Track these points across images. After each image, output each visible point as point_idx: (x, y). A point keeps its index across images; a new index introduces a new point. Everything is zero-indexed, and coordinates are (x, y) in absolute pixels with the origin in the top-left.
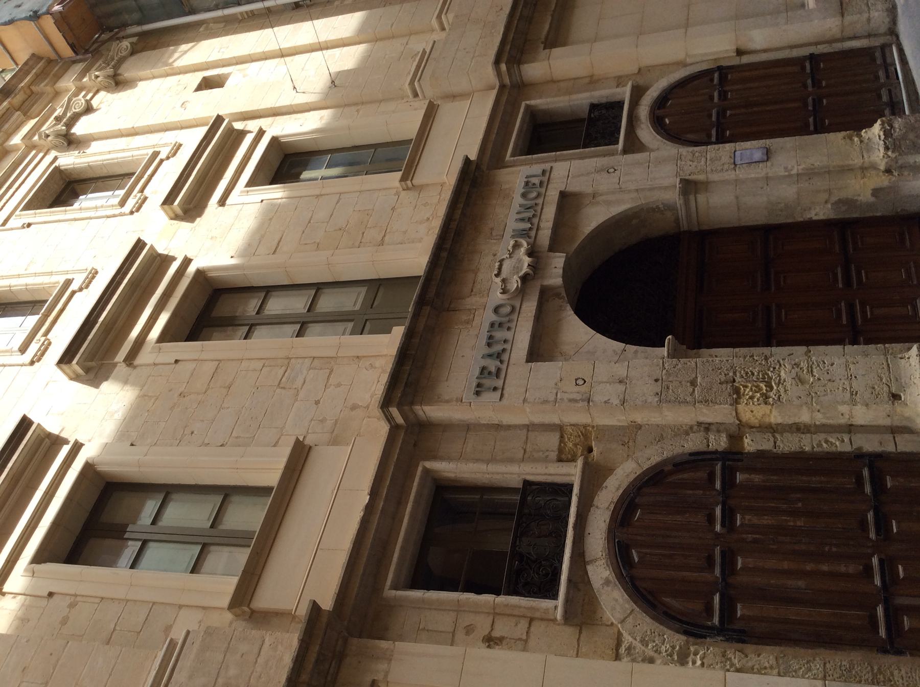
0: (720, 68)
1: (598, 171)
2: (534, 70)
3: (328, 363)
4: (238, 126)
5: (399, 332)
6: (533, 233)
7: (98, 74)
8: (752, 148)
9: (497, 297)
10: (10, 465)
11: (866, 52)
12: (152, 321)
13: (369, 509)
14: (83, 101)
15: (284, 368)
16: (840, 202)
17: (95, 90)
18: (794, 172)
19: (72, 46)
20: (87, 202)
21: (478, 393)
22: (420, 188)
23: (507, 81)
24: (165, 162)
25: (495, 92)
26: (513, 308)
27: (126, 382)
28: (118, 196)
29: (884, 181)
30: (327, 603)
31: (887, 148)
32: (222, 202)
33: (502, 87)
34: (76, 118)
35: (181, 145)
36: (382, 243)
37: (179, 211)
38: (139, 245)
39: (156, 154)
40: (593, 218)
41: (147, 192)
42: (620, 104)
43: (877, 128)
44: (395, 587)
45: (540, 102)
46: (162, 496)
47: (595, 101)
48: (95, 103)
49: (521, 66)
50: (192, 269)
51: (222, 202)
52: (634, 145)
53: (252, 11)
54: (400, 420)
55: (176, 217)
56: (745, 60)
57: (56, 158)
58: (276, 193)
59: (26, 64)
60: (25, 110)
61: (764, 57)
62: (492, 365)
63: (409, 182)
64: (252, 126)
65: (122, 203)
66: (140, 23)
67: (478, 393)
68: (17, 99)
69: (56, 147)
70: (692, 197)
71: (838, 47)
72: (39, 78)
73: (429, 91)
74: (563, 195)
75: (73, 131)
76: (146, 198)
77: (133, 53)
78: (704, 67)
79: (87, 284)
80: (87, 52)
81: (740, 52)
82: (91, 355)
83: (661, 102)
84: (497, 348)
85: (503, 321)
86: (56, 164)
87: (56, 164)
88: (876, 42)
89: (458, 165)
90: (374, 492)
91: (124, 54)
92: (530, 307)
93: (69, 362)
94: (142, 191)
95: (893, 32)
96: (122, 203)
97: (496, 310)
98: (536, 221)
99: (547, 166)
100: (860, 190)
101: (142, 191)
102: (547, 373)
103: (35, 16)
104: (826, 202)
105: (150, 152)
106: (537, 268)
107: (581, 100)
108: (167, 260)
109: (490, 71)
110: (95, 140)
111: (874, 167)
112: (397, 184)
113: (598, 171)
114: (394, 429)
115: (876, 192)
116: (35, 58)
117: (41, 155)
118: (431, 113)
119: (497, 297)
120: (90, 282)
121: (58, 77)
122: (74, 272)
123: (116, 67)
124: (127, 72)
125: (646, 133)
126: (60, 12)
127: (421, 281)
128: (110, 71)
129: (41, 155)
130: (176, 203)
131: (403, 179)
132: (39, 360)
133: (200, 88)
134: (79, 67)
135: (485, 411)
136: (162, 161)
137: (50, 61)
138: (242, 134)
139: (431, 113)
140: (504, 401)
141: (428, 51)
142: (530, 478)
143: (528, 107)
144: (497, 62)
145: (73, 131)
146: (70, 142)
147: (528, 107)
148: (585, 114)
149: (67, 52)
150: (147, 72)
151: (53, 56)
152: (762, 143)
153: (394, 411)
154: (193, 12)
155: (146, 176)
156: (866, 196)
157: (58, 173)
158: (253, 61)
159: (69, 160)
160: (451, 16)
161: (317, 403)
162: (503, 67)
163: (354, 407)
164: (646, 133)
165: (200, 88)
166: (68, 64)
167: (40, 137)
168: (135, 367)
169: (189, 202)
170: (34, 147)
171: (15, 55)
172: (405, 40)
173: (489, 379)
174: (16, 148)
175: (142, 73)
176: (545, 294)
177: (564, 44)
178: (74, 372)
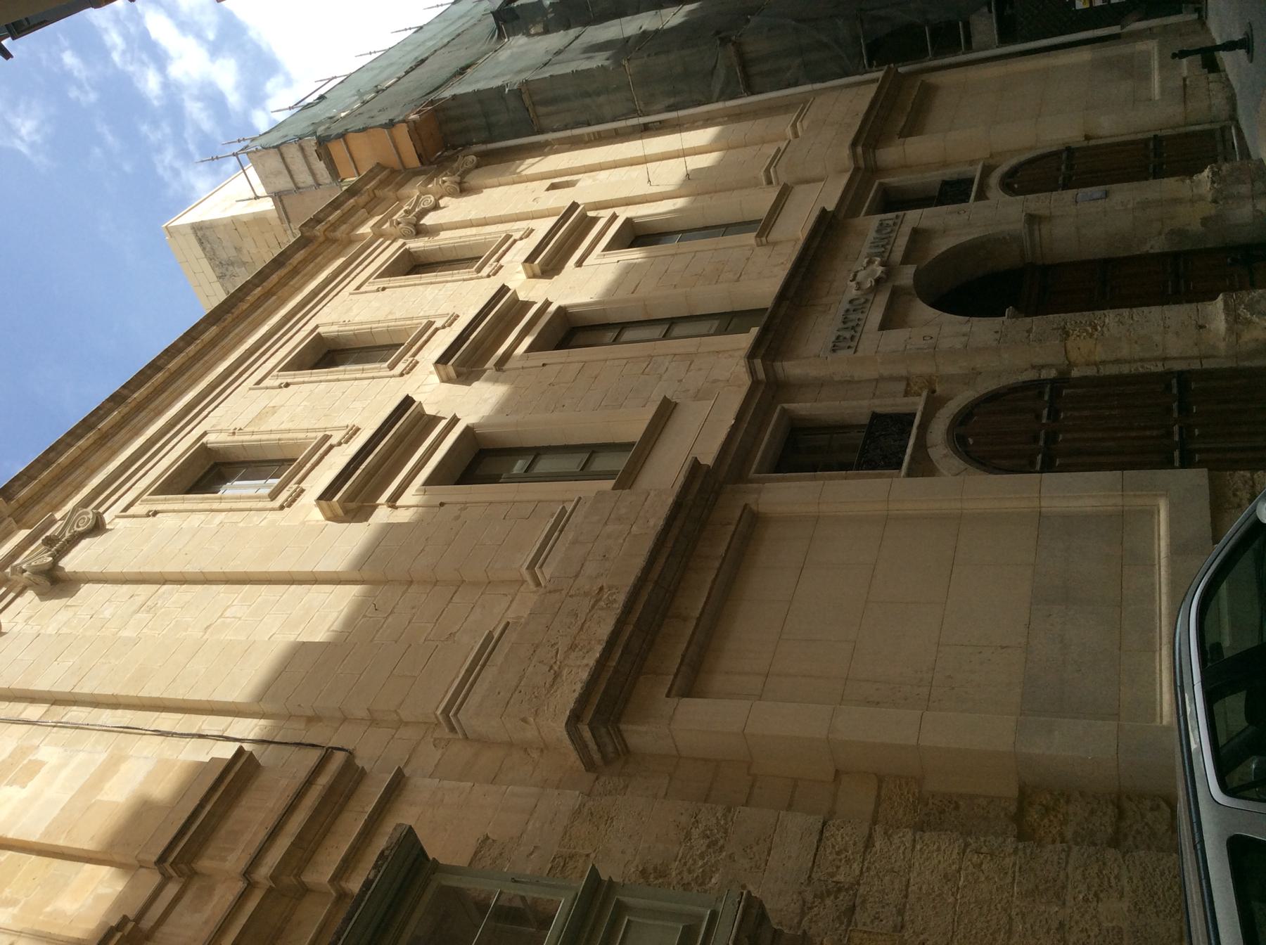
0: (1068, 149)
1: (951, 213)
2: (890, 154)
3: (690, 357)
4: (591, 214)
5: (755, 331)
6: (886, 255)
7: (446, 180)
8: (1096, 191)
9: (853, 292)
10: (397, 426)
11: (1211, 133)
12: (517, 342)
13: (734, 428)
14: (91, 516)
15: (510, 598)
16: (1172, 232)
17: (18, 589)
18: (1130, 206)
19: (420, 157)
20: (235, 489)
21: (834, 349)
22: (775, 244)
23: (862, 163)
24: (335, 449)
25: (847, 176)
26: (867, 301)
27: (495, 380)
28: (269, 486)
29: (1211, 210)
30: (708, 460)
31: (1213, 182)
32: (579, 263)
33: (857, 169)
34: (424, 212)
35: (358, 429)
36: (738, 280)
37: (538, 271)
38: (408, 402)
39: (430, 324)
40: (942, 245)
41: (502, 262)
42: (971, 181)
43: (1207, 172)
44: (758, 471)
45: (803, 407)
46: (531, 458)
47: (946, 178)
48: (442, 202)
49: (877, 152)
50: (552, 308)
51: (579, 263)
52: (923, 467)
53: (599, 133)
54: (761, 375)
55: (334, 518)
56: (1092, 143)
57: (404, 244)
58: (634, 255)
59: (371, 171)
60: (371, 207)
61: (1109, 141)
62: (848, 334)
63: (764, 239)
64: (605, 214)
65: (273, 495)
66: (485, 142)
67: (834, 349)
68: (362, 199)
69: (404, 236)
70: (1036, 227)
71: (1182, 130)
72: (383, 184)
73: (783, 175)
74: (915, 231)
75: (61, 564)
76: (501, 267)
77: (477, 166)
78: (1054, 149)
79: (348, 439)
80: (431, 163)
81: (1087, 138)
82: (350, 497)
83: (964, 418)
84: (850, 324)
85: (857, 306)
86: (204, 440)
87: (204, 440)
88: (1217, 126)
89: (816, 213)
90: (739, 418)
91: (470, 166)
92: (882, 300)
93: (446, 363)
94: (498, 260)
95: (1233, 118)
96: (273, 495)
97: (851, 302)
98: (889, 247)
99: (901, 213)
100: (1191, 218)
101: (498, 260)
102: (896, 337)
103: (391, 124)
104: (1160, 234)
105: (320, 435)
106: (890, 270)
107: (858, 408)
108: (527, 305)
109: (846, 152)
110: (88, 581)
111: (1202, 198)
112: (753, 241)
113: (951, 213)
114: (755, 383)
115: (1205, 221)
116: (380, 167)
117: (12, 595)
118: (785, 193)
119: (853, 292)
120: (294, 500)
121: (401, 185)
122: (436, 316)
123: (463, 175)
124: (472, 180)
125: (939, 449)
126: (414, 121)
127: (767, 314)
128: (457, 179)
129: (12, 595)
130: (336, 499)
131: (759, 236)
132: (289, 506)
133: (548, 190)
134: (421, 179)
135: (840, 366)
136: (331, 447)
137: (394, 172)
138: (595, 220)
139: (785, 193)
140: (858, 354)
141: (496, 635)
142: (878, 410)
143: (881, 184)
144: (854, 144)
145: (61, 564)
146: (420, 231)
147: (881, 184)
148: (865, 420)
149: (413, 161)
150: (495, 181)
151: (398, 166)
152: (1102, 187)
153: (758, 362)
154: (541, 131)
155: (308, 465)
156: (1196, 226)
157: (407, 254)
158: (602, 169)
159: (416, 244)
160: (805, 123)
161: (680, 381)
162: (859, 150)
163: (715, 381)
164: (939, 449)
165: (548, 190)
166: (416, 173)
167: (14, 569)
168: (396, 508)
169: (548, 262)
170: (381, 236)
171: (359, 165)
172: (756, 148)
173: (847, 338)
174: (363, 236)
175: (489, 181)
176: (896, 293)
177: (921, 134)
178: (447, 375)
